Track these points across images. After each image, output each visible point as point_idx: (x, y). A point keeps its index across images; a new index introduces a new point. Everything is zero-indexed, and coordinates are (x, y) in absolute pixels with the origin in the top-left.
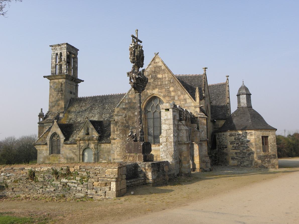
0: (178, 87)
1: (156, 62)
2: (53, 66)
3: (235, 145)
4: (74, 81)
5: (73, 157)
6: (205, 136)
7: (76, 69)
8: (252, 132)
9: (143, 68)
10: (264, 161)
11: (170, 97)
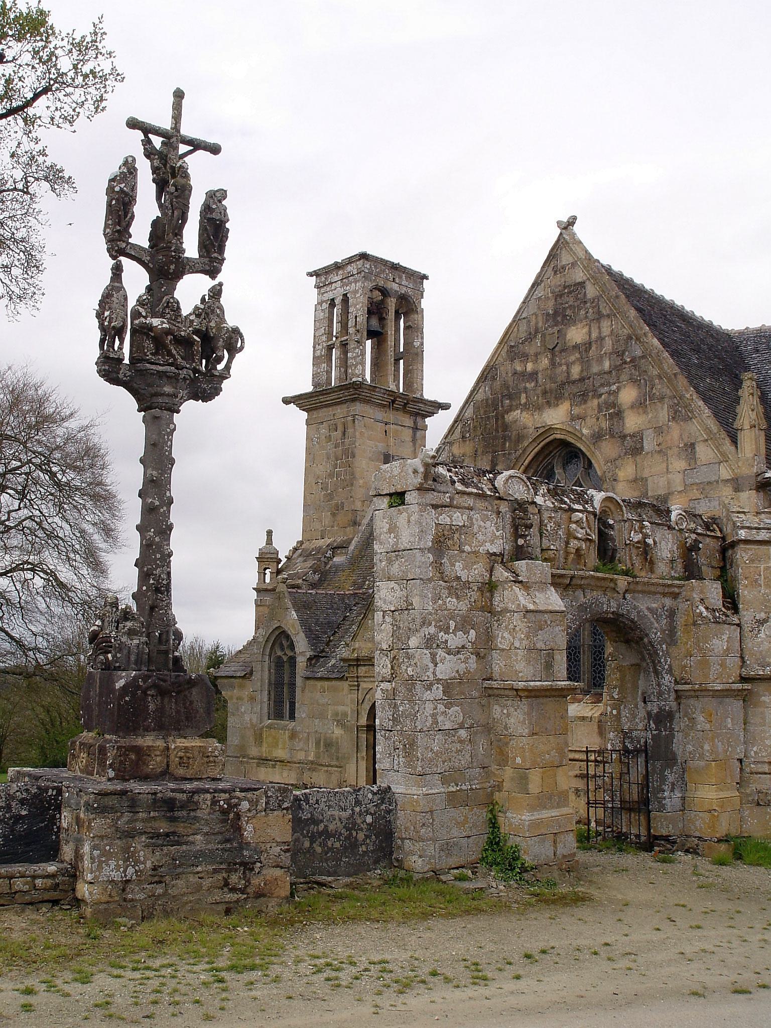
1: (563, 268)
2: (318, 353)
9: (220, 278)
11: (624, 437)
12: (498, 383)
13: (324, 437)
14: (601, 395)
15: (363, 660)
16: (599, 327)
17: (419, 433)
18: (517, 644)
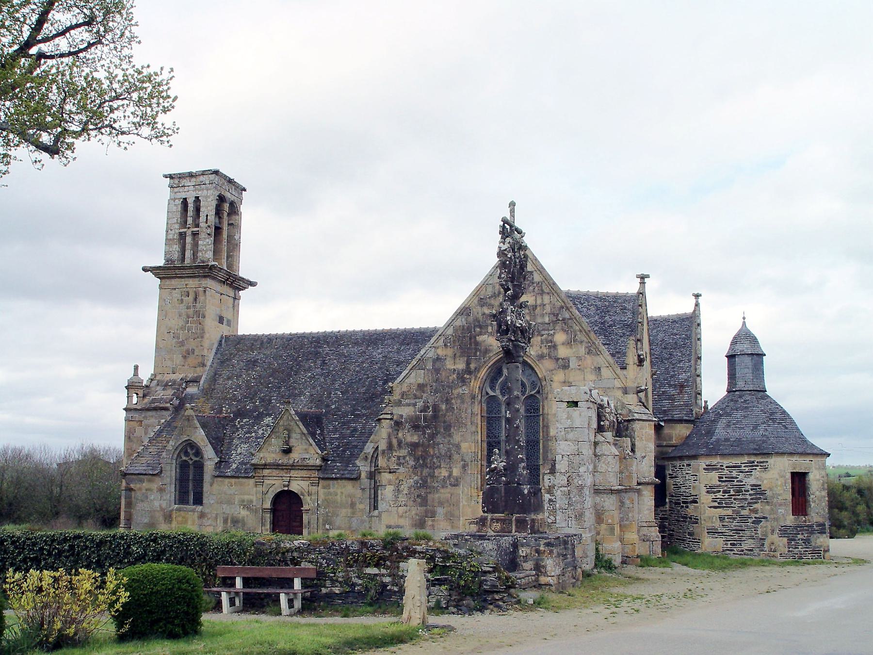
0: (578, 333)
2: (171, 237)
3: (719, 495)
4: (231, 285)
5: (243, 517)
6: (650, 471)
7: (234, 246)
8: (767, 462)
10: (794, 540)
11: (557, 359)
12: (471, 318)
13: (176, 300)
14: (543, 335)
15: (269, 465)
16: (542, 299)
17: (236, 301)
18: (610, 470)
